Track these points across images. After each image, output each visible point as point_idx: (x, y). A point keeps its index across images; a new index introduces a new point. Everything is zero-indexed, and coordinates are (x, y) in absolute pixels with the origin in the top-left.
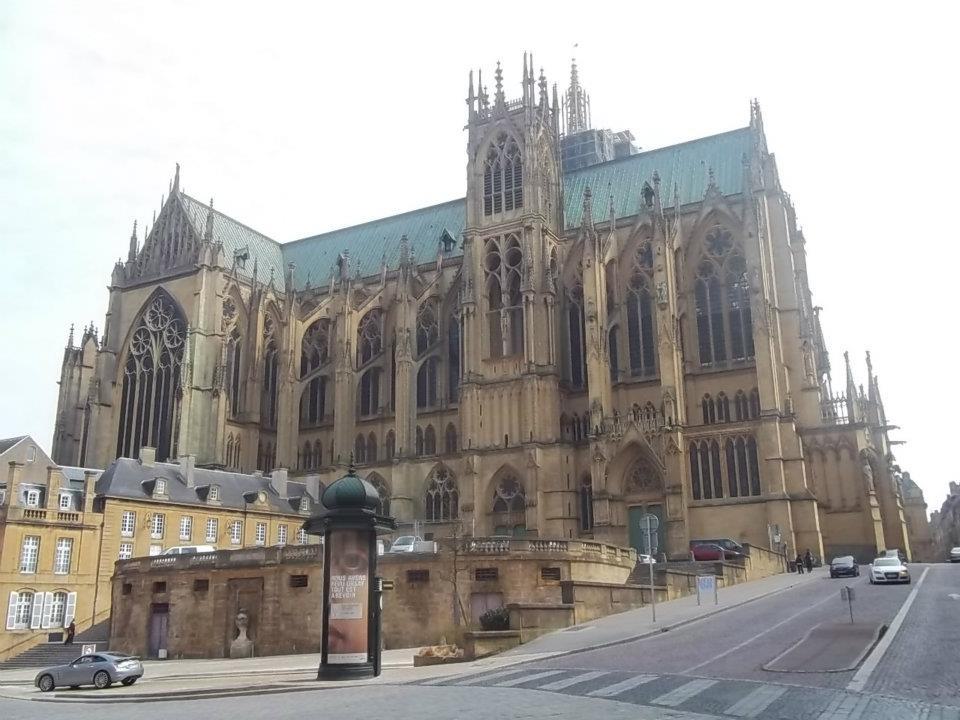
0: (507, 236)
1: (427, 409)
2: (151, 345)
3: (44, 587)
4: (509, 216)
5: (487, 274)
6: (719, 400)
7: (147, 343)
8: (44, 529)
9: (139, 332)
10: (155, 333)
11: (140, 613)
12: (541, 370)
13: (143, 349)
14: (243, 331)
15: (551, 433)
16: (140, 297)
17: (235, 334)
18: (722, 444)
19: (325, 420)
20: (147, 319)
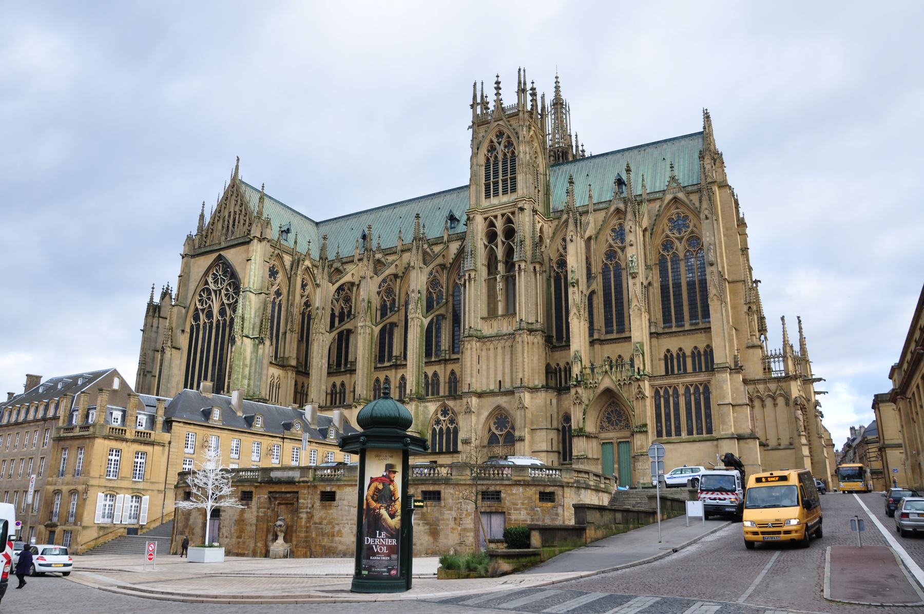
0: (503, 215)
2: (212, 301)
3: (123, 491)
4: (505, 199)
5: (486, 246)
6: (678, 354)
7: (209, 299)
8: (124, 443)
9: (203, 290)
10: (215, 291)
13: (206, 304)
14: (284, 291)
15: (539, 380)
16: (206, 262)
17: (278, 293)
18: (681, 390)
20: (210, 280)
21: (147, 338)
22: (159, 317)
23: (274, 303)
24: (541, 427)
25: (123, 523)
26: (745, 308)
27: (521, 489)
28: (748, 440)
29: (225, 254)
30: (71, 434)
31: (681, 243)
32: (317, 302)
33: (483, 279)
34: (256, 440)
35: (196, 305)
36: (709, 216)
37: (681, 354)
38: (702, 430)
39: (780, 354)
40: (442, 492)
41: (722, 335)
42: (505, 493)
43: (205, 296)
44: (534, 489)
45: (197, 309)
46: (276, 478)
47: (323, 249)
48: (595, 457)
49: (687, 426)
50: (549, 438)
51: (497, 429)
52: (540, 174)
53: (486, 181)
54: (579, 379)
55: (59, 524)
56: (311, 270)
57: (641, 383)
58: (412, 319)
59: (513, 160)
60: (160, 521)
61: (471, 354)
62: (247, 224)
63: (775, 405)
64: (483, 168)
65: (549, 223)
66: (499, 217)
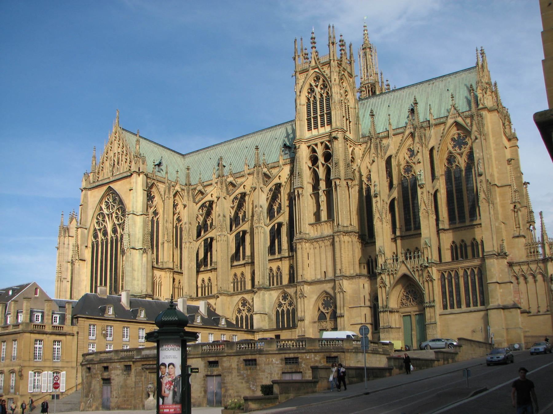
0: (322, 143)
1: (277, 256)
2: (106, 223)
3: (47, 369)
4: (322, 130)
5: (310, 168)
6: (461, 246)
7: (104, 221)
8: (45, 335)
9: (99, 214)
10: (108, 215)
11: (97, 384)
12: (345, 229)
13: (102, 225)
18: (461, 273)
19: (213, 265)
20: (104, 206)
21: (61, 253)
22: (69, 236)
23: (152, 221)
24: (357, 306)
25: (48, 391)
26: (512, 206)
27: (313, 355)
28: (511, 310)
29: (114, 186)
30: (7, 331)
31: (461, 157)
32: (185, 219)
33: (309, 194)
34: (141, 327)
35: (94, 226)
36: (478, 136)
37: (463, 244)
38: (477, 303)
39: (539, 241)
40: (257, 359)
41: (490, 229)
42: (301, 359)
43: (101, 219)
44: (322, 354)
45: (95, 230)
46: (146, 355)
47: (188, 176)
48: (398, 326)
49: (466, 300)
50: (363, 314)
51: (324, 308)
52: (351, 108)
53: (307, 117)
54: (383, 268)
55: (4, 394)
56: (180, 193)
57: (429, 269)
58: (257, 227)
59: (328, 100)
60: (75, 389)
61: (302, 253)
62: (128, 161)
63: (535, 281)
64: (305, 107)
65: (359, 146)
66: (319, 145)
